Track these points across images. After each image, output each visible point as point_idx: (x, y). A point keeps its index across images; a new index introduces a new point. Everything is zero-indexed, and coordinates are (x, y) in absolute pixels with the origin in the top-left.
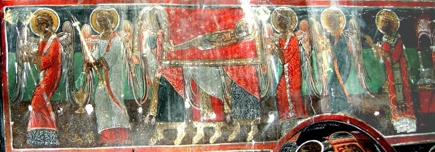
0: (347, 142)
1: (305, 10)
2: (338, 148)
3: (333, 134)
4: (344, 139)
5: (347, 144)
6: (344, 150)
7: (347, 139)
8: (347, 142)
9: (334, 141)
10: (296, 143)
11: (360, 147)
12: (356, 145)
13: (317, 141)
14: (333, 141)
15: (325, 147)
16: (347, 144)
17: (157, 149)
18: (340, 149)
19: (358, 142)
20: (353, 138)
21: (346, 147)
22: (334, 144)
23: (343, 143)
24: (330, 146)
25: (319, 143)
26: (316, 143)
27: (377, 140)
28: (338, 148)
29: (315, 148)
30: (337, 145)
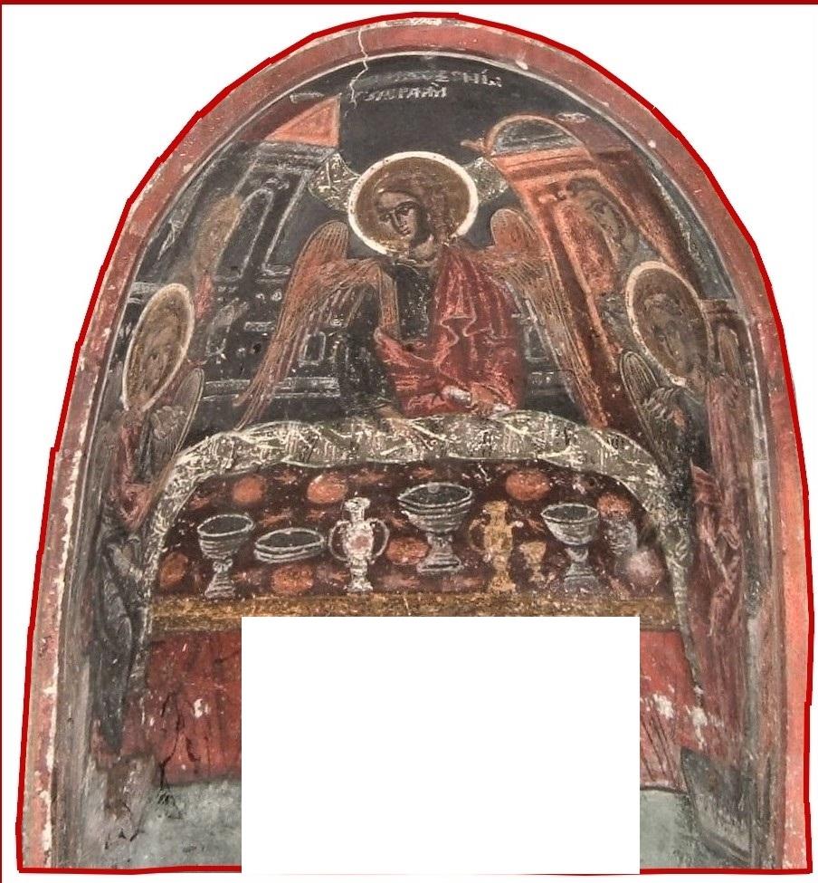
0: (562, 168)
1: (273, 170)
2: (535, 195)
3: (497, 128)
4: (545, 154)
5: (567, 176)
6: (562, 204)
7: (557, 152)
8: (562, 168)
9: (512, 163)
10: (337, 157)
11: (610, 189)
12: (593, 180)
13: (440, 158)
14: (508, 160)
15: (482, 187)
16: (567, 176)
17: (421, 59)
18: (542, 200)
19: (600, 169)
20: (577, 148)
21: (563, 193)
22: (517, 176)
23: (548, 170)
24: (503, 186)
25: (460, 171)
26: (436, 165)
27: (648, 148)
28: (535, 195)
29: (439, 190)
30: (530, 183)
